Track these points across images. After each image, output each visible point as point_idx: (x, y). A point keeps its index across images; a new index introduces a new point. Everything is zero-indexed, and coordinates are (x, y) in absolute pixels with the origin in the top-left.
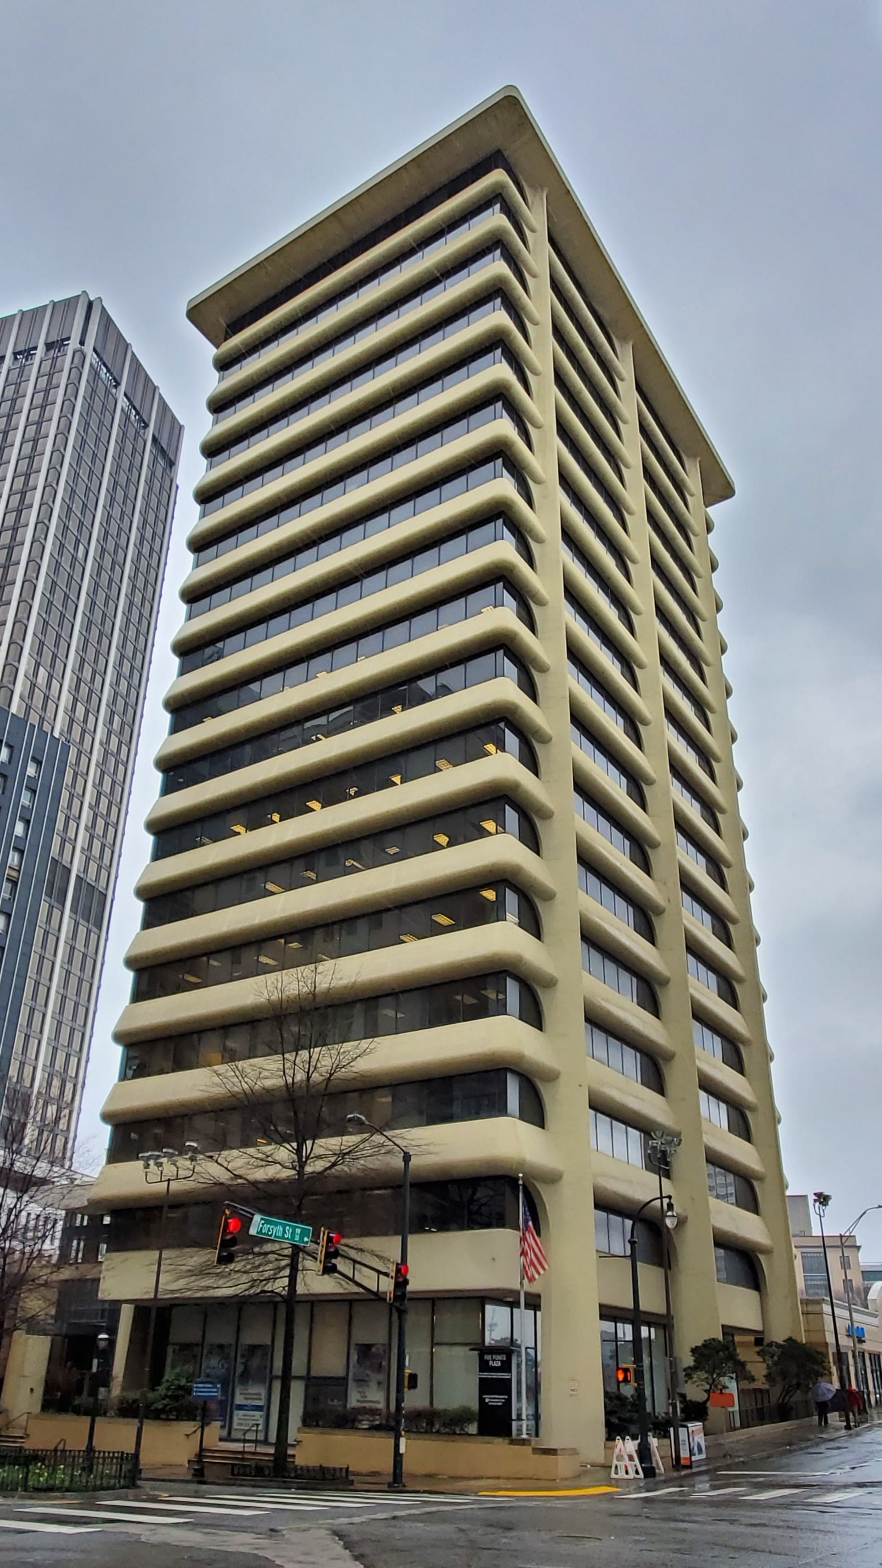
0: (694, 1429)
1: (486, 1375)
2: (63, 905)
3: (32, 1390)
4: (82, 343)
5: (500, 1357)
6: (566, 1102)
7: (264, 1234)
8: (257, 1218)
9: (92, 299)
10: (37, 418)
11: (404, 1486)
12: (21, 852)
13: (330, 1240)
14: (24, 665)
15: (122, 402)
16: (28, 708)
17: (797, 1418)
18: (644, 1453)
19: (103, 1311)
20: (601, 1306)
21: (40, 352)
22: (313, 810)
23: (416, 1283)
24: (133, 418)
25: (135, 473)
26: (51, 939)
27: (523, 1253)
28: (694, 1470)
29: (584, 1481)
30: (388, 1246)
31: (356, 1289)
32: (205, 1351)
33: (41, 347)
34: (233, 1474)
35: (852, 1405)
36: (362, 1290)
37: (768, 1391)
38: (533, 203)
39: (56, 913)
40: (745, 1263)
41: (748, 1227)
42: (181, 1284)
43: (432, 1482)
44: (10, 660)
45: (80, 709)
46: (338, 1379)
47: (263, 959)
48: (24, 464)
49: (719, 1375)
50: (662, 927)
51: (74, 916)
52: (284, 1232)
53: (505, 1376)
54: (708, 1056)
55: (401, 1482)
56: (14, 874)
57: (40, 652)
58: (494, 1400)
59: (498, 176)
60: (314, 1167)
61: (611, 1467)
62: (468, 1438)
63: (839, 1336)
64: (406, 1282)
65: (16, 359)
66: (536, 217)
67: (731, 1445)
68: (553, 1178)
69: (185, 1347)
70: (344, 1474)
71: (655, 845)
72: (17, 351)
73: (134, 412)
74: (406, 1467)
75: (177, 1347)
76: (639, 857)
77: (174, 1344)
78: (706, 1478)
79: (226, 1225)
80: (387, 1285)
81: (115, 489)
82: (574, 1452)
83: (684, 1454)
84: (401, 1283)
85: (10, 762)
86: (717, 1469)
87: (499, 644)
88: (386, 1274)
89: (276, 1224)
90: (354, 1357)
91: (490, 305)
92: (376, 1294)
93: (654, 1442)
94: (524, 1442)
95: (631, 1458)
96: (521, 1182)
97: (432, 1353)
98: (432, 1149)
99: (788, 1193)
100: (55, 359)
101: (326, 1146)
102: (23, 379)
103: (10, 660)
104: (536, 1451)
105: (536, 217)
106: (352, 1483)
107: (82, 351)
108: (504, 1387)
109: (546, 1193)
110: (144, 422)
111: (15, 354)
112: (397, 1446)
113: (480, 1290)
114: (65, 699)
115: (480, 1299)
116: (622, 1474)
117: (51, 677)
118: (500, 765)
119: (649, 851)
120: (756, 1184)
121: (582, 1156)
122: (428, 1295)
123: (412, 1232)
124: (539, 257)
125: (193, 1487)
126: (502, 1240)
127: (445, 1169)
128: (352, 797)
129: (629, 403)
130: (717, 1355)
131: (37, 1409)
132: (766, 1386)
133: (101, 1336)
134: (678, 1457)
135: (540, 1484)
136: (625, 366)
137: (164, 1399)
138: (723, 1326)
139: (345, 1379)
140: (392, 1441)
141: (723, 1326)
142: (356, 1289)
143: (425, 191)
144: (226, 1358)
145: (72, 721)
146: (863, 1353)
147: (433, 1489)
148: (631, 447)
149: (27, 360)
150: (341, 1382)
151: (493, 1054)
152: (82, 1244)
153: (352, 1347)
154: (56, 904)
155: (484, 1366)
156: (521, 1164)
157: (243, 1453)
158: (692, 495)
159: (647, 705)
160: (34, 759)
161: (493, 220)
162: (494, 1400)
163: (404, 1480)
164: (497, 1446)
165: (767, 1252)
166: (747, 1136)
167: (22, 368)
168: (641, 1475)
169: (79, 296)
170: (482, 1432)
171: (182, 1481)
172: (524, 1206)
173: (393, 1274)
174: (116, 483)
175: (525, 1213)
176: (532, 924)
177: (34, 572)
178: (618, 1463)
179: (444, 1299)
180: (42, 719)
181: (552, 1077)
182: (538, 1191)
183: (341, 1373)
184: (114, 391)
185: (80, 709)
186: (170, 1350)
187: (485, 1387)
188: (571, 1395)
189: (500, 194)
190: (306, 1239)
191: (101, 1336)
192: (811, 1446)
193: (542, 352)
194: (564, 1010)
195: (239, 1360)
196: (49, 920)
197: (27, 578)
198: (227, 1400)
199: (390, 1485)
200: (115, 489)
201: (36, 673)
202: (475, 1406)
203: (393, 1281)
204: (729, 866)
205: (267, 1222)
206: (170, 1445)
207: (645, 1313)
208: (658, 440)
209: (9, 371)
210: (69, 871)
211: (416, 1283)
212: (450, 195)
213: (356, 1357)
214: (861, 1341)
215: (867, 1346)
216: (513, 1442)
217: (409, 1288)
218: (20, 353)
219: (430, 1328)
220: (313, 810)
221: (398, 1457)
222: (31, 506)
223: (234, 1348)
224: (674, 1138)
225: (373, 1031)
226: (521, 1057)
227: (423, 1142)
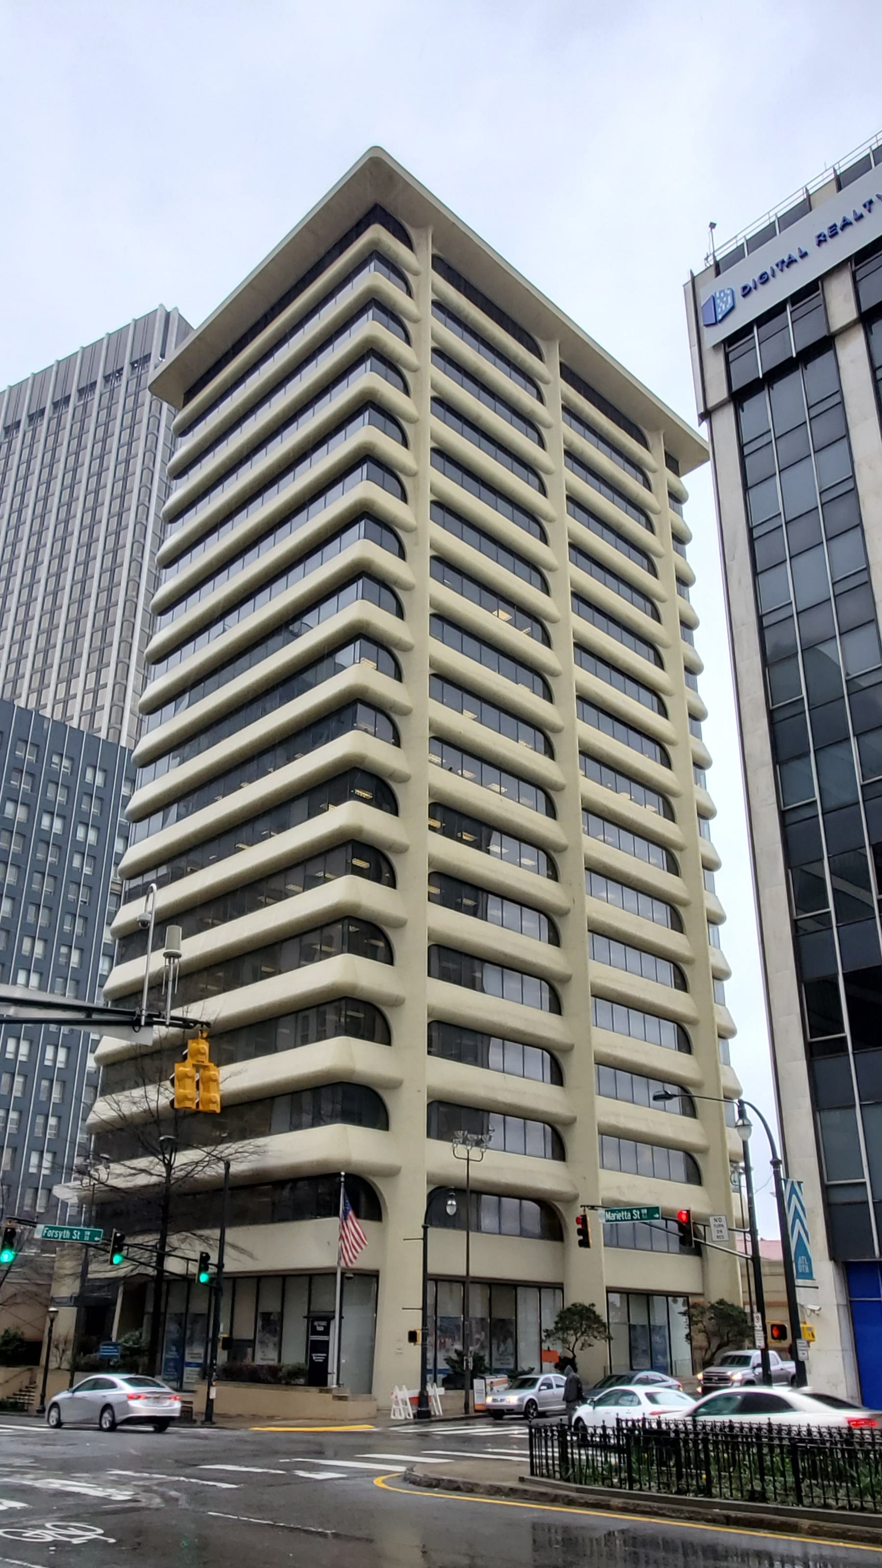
9: (169, 310)
27: (341, 1237)
44: (119, 679)
46: (250, 1341)
53: (324, 1338)
56: (118, 888)
58: (318, 1357)
60: (177, 1174)
74: (216, 1410)
85: (105, 785)
90: (260, 1323)
101: (183, 1158)
102: (113, 402)
103: (119, 679)
108: (323, 1347)
122: (308, 1272)
135: (337, 1422)
136: (547, 370)
139: (254, 1341)
143: (322, 251)
150: (252, 1343)
162: (318, 1357)
169: (156, 310)
175: (345, 1205)
177: (133, 591)
179: (242, 1278)
183: (252, 1337)
188: (398, 1353)
190: (96, 1239)
197: (128, 597)
209: (101, 396)
212: (341, 252)
222: (127, 527)
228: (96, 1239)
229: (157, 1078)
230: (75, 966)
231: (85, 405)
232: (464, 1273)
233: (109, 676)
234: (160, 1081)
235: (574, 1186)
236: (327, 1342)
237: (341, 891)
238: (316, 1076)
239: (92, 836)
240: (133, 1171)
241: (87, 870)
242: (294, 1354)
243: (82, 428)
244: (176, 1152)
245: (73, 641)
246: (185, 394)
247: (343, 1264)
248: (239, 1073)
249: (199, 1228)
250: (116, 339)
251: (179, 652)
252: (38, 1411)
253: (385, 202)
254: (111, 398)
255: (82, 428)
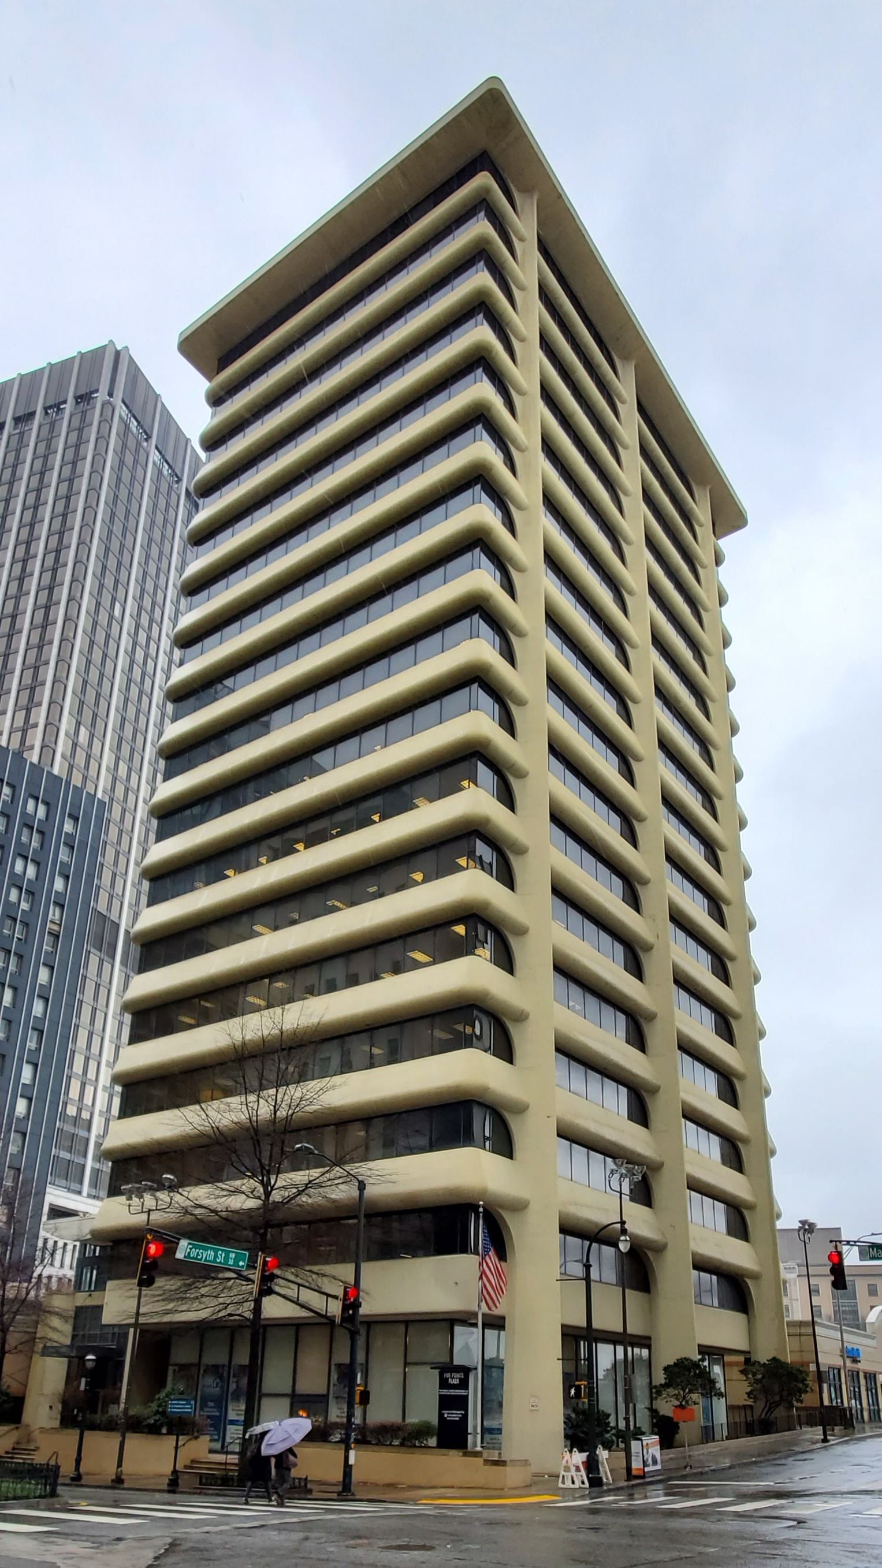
0: (649, 1442)
1: (445, 1392)
2: (113, 958)
3: (51, 1407)
4: (111, 395)
5: (458, 1375)
6: (534, 1134)
7: (193, 1258)
8: (184, 1243)
9: (119, 348)
10: (68, 474)
11: (353, 1495)
12: (62, 906)
13: (265, 1263)
14: (66, 724)
15: (155, 456)
16: (71, 767)
17: (777, 1432)
18: (592, 1465)
19: (114, 1334)
20: (563, 1326)
21: (68, 407)
22: (298, 851)
23: (367, 1308)
24: (165, 472)
25: (169, 528)
26: (103, 991)
28: (648, 1480)
29: (534, 1489)
30: (346, 1271)
31: (304, 1313)
32: (202, 1371)
33: (70, 399)
34: (201, 1483)
35: (837, 1421)
36: (313, 1314)
37: (751, 1407)
38: (522, 210)
39: (107, 966)
40: (735, 1289)
41: (736, 1254)
42: (160, 1307)
43: (386, 1491)
45: (123, 768)
46: (323, 1396)
47: (250, 999)
48: (28, 514)
49: (690, 1391)
50: (650, 964)
51: (124, 969)
52: (216, 1256)
54: (700, 1089)
55: (350, 1491)
56: (56, 928)
57: (80, 711)
58: (454, 1415)
59: (483, 179)
60: (276, 1196)
61: (558, 1477)
62: (429, 1451)
63: (819, 1354)
64: (356, 1305)
65: (47, 413)
66: (526, 226)
67: (701, 1457)
68: (519, 1207)
69: (183, 1367)
70: (303, 1484)
71: (645, 882)
72: (48, 405)
73: (167, 467)
74: (355, 1476)
75: (176, 1368)
76: (716, 913)
77: (176, 1365)
78: (660, 1486)
79: (147, 1249)
80: (335, 1308)
81: (149, 546)
82: (526, 1463)
83: (636, 1465)
84: (351, 1305)
85: (47, 819)
86: (670, 1479)
87: (473, 678)
88: (336, 1297)
89: (206, 1249)
90: (334, 1376)
91: (472, 322)
92: (325, 1317)
93: (603, 1454)
94: (477, 1454)
95: (578, 1469)
96: (481, 1210)
97: (405, 1373)
98: (394, 1178)
99: (780, 1225)
100: (84, 413)
104: (487, 1462)
105: (526, 226)
106: (310, 1491)
107: (109, 403)
108: (462, 1403)
109: (511, 1221)
110: (177, 476)
111: (46, 409)
112: (347, 1458)
113: (448, 1313)
114: (108, 758)
115: (450, 1322)
116: (568, 1484)
117: (92, 736)
118: (473, 800)
119: (638, 887)
120: (746, 1212)
121: (547, 1184)
123: (370, 1258)
124: (528, 268)
125: (167, 1496)
126: (462, 1267)
127: (412, 1197)
128: (333, 837)
129: (629, 427)
130: (689, 1375)
131: (57, 1424)
132: (750, 1402)
133: (89, 1357)
134: (629, 1469)
136: (626, 388)
137: (155, 1415)
138: (699, 1345)
140: (343, 1452)
141: (699, 1345)
142: (304, 1313)
144: (221, 1377)
145: (115, 779)
146: (858, 1373)
147: (375, 1497)
148: (631, 473)
149: (57, 414)
151: (457, 1086)
152: (95, 1272)
153: (333, 1368)
154: (106, 958)
155: (444, 1384)
156: (483, 1193)
157: (226, 1464)
158: (701, 525)
159: (639, 740)
160: (70, 816)
161: (480, 227)
162: (454, 1415)
163: (352, 1488)
164: (453, 1458)
165: (756, 1276)
166: (739, 1168)
167: (52, 424)
168: (587, 1485)
170: (441, 1445)
171: (159, 1491)
172: (483, 1232)
173: (341, 1296)
174: (150, 540)
176: (505, 960)
178: (565, 1474)
180: (85, 778)
181: (521, 1109)
182: (505, 1222)
183: (322, 1391)
184: (145, 444)
185: (123, 768)
186: (171, 1369)
187: (445, 1403)
188: (532, 1411)
189: (484, 200)
190: (241, 1263)
191: (89, 1357)
192: (780, 1458)
193: (529, 369)
194: (534, 1042)
195: (231, 1379)
196: (99, 974)
198: (220, 1416)
199: (339, 1494)
200: (149, 546)
201: (77, 732)
202: (435, 1421)
203: (341, 1304)
204: (728, 904)
205: (195, 1247)
206: (152, 1456)
207: (597, 1330)
208: (663, 467)
210: (118, 926)
211: (367, 1308)
213: (336, 1377)
214: (855, 1361)
215: (863, 1366)
216: (465, 1454)
217: (362, 1311)
218: (50, 407)
219: (403, 1348)
220: (298, 851)
221: (348, 1469)
223: (226, 1368)
224: (656, 1167)
225: (347, 1067)
226: (486, 1089)
227: (385, 1172)
228: (241, 1263)
229: (256, 1084)
230: (8, 1005)
231: (22, 435)
232: (584, 1324)
233: (40, 715)
234: (262, 1088)
235: (663, 1234)
236: (466, 1398)
237: (468, 884)
238: (439, 1093)
239: (31, 871)
240: (225, 1193)
241: (24, 906)
242: (425, 1409)
243: (17, 458)
244: (278, 1173)
245: (39, 647)
246: (219, 360)
247: (484, 1309)
248: (333, 1087)
249: (309, 1264)
250: (60, 371)
251: (219, 634)
252: (72, 1479)
253: (495, 153)
254: (52, 430)
255: (17, 458)
